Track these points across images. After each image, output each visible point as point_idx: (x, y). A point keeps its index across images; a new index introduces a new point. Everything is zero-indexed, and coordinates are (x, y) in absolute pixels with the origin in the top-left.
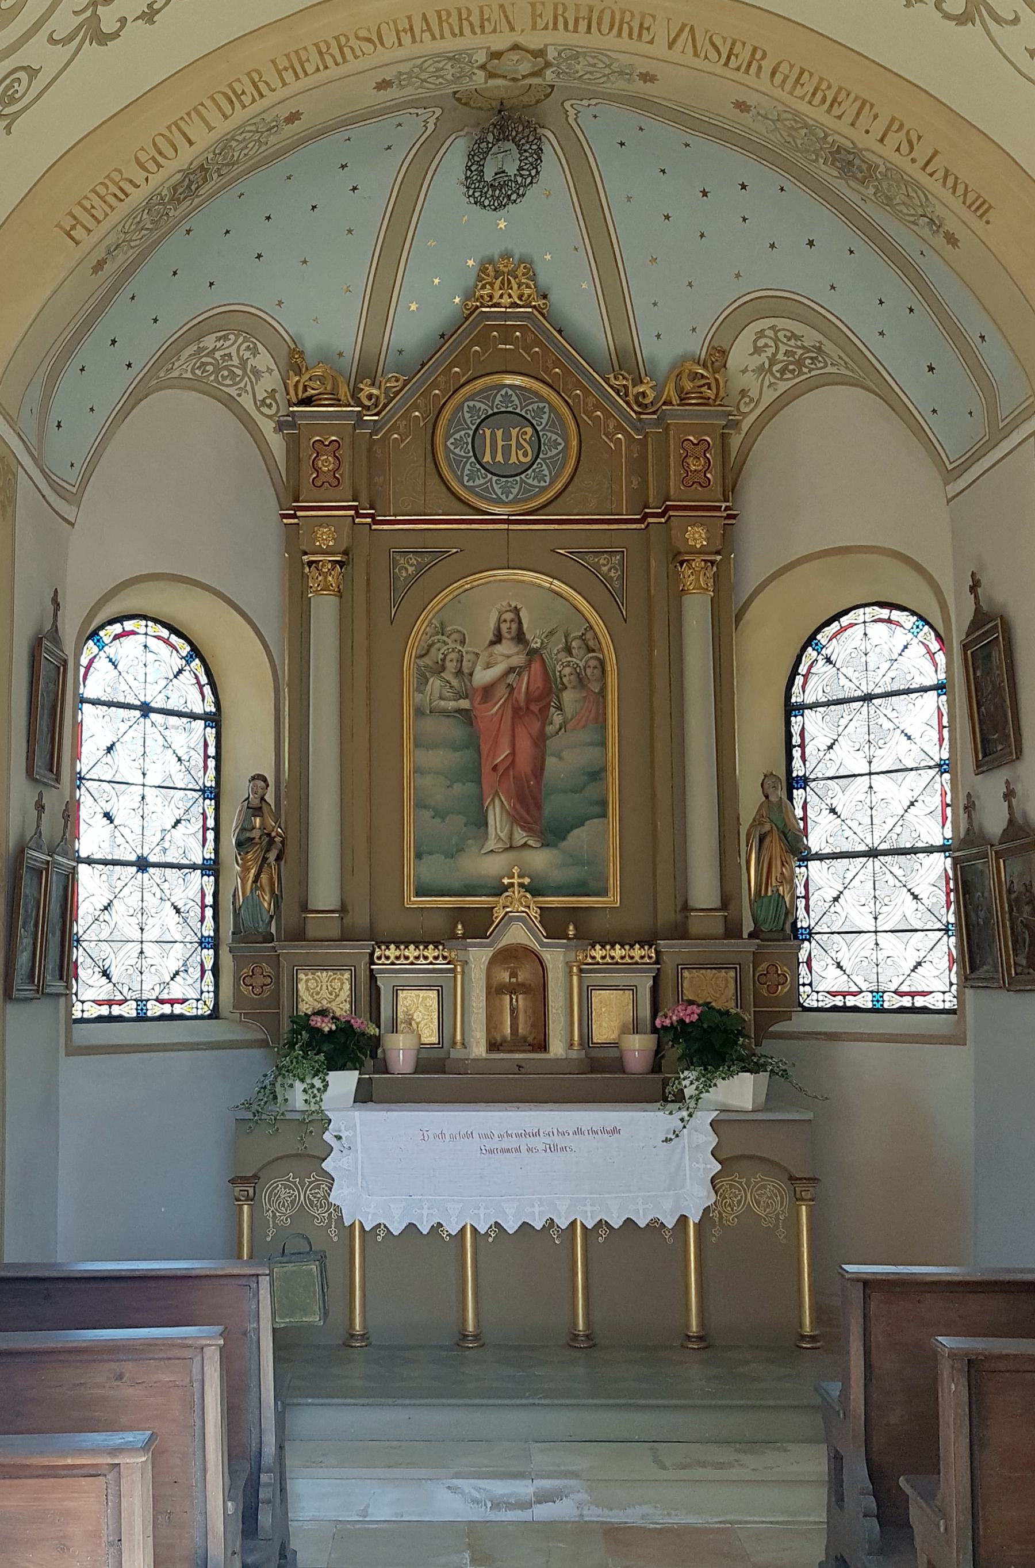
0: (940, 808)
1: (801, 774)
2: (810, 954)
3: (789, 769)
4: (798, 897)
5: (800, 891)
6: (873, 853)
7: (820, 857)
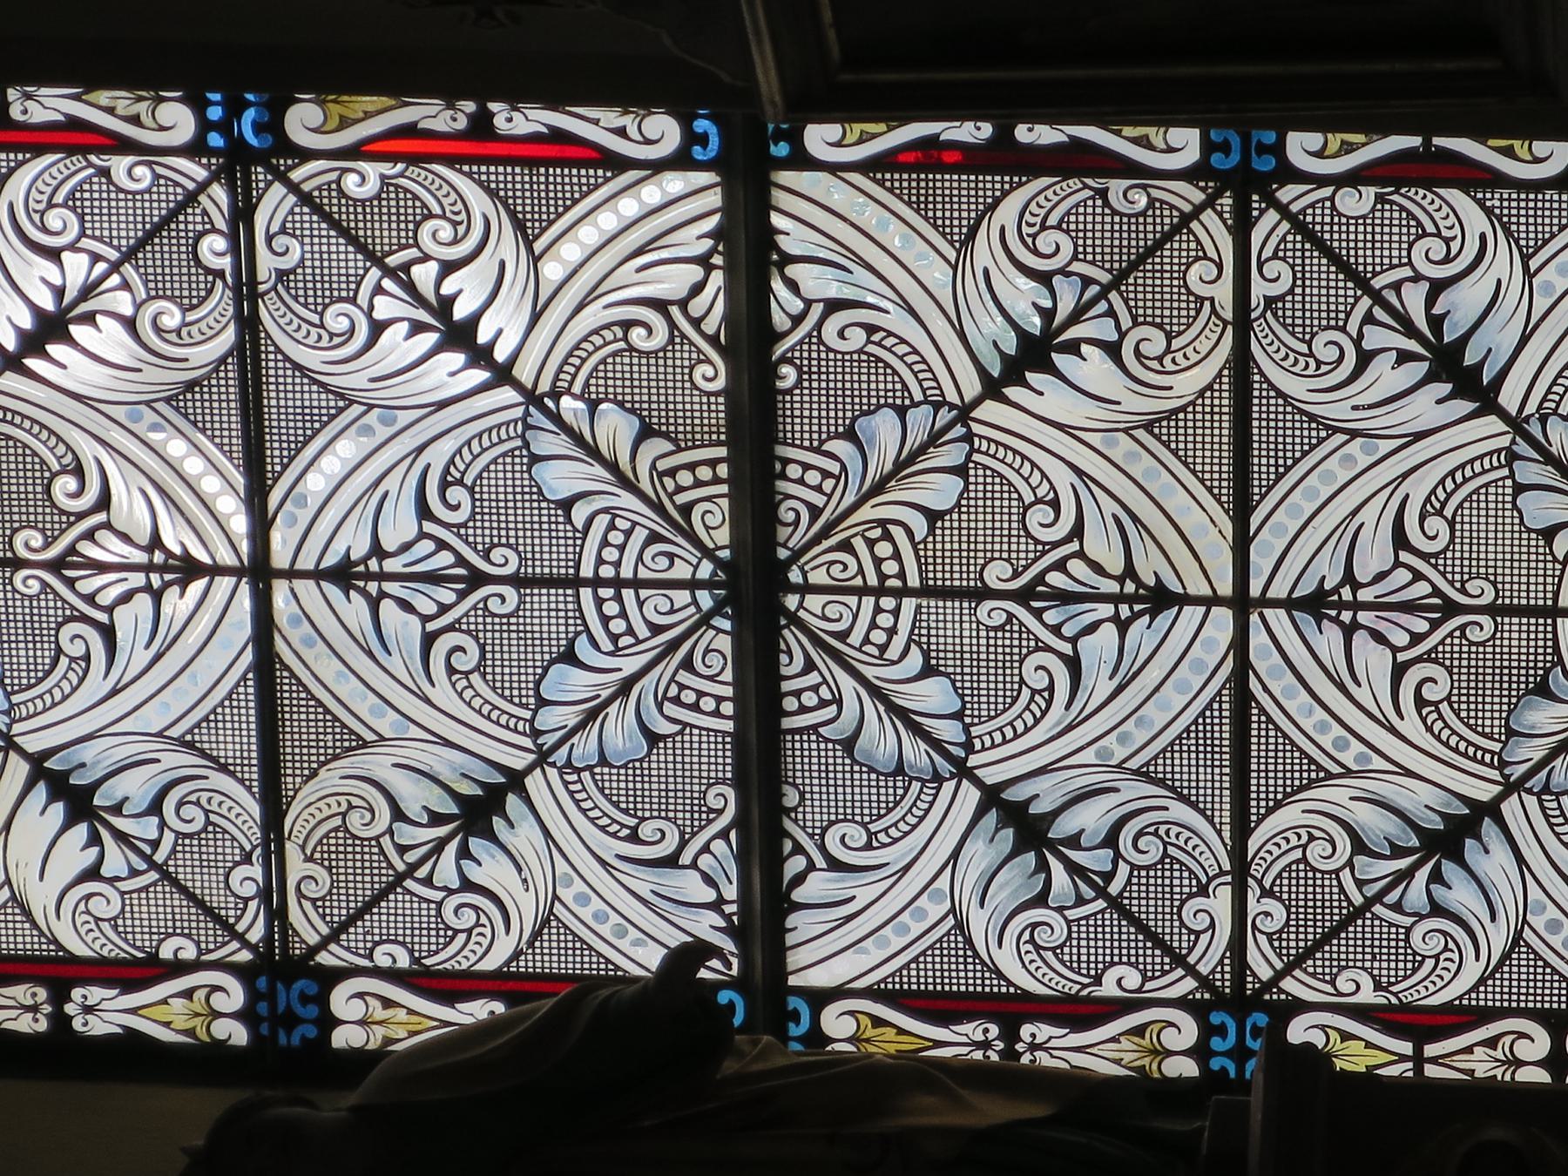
0: (496, 174)
1: (234, 996)
2: (1362, 1013)
3: (199, 1061)
4: (1010, 1054)
5: (961, 1041)
6: (755, 590)
7: (765, 912)
